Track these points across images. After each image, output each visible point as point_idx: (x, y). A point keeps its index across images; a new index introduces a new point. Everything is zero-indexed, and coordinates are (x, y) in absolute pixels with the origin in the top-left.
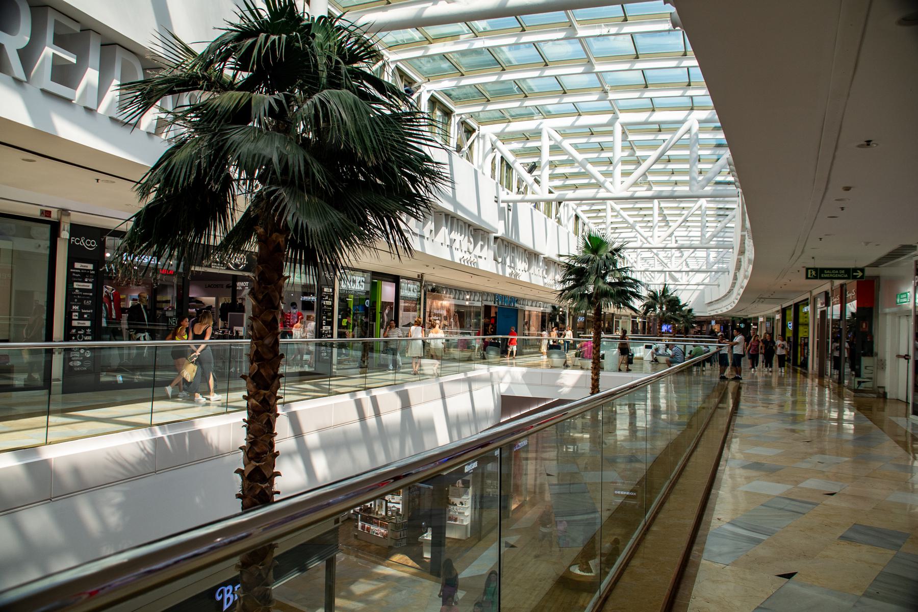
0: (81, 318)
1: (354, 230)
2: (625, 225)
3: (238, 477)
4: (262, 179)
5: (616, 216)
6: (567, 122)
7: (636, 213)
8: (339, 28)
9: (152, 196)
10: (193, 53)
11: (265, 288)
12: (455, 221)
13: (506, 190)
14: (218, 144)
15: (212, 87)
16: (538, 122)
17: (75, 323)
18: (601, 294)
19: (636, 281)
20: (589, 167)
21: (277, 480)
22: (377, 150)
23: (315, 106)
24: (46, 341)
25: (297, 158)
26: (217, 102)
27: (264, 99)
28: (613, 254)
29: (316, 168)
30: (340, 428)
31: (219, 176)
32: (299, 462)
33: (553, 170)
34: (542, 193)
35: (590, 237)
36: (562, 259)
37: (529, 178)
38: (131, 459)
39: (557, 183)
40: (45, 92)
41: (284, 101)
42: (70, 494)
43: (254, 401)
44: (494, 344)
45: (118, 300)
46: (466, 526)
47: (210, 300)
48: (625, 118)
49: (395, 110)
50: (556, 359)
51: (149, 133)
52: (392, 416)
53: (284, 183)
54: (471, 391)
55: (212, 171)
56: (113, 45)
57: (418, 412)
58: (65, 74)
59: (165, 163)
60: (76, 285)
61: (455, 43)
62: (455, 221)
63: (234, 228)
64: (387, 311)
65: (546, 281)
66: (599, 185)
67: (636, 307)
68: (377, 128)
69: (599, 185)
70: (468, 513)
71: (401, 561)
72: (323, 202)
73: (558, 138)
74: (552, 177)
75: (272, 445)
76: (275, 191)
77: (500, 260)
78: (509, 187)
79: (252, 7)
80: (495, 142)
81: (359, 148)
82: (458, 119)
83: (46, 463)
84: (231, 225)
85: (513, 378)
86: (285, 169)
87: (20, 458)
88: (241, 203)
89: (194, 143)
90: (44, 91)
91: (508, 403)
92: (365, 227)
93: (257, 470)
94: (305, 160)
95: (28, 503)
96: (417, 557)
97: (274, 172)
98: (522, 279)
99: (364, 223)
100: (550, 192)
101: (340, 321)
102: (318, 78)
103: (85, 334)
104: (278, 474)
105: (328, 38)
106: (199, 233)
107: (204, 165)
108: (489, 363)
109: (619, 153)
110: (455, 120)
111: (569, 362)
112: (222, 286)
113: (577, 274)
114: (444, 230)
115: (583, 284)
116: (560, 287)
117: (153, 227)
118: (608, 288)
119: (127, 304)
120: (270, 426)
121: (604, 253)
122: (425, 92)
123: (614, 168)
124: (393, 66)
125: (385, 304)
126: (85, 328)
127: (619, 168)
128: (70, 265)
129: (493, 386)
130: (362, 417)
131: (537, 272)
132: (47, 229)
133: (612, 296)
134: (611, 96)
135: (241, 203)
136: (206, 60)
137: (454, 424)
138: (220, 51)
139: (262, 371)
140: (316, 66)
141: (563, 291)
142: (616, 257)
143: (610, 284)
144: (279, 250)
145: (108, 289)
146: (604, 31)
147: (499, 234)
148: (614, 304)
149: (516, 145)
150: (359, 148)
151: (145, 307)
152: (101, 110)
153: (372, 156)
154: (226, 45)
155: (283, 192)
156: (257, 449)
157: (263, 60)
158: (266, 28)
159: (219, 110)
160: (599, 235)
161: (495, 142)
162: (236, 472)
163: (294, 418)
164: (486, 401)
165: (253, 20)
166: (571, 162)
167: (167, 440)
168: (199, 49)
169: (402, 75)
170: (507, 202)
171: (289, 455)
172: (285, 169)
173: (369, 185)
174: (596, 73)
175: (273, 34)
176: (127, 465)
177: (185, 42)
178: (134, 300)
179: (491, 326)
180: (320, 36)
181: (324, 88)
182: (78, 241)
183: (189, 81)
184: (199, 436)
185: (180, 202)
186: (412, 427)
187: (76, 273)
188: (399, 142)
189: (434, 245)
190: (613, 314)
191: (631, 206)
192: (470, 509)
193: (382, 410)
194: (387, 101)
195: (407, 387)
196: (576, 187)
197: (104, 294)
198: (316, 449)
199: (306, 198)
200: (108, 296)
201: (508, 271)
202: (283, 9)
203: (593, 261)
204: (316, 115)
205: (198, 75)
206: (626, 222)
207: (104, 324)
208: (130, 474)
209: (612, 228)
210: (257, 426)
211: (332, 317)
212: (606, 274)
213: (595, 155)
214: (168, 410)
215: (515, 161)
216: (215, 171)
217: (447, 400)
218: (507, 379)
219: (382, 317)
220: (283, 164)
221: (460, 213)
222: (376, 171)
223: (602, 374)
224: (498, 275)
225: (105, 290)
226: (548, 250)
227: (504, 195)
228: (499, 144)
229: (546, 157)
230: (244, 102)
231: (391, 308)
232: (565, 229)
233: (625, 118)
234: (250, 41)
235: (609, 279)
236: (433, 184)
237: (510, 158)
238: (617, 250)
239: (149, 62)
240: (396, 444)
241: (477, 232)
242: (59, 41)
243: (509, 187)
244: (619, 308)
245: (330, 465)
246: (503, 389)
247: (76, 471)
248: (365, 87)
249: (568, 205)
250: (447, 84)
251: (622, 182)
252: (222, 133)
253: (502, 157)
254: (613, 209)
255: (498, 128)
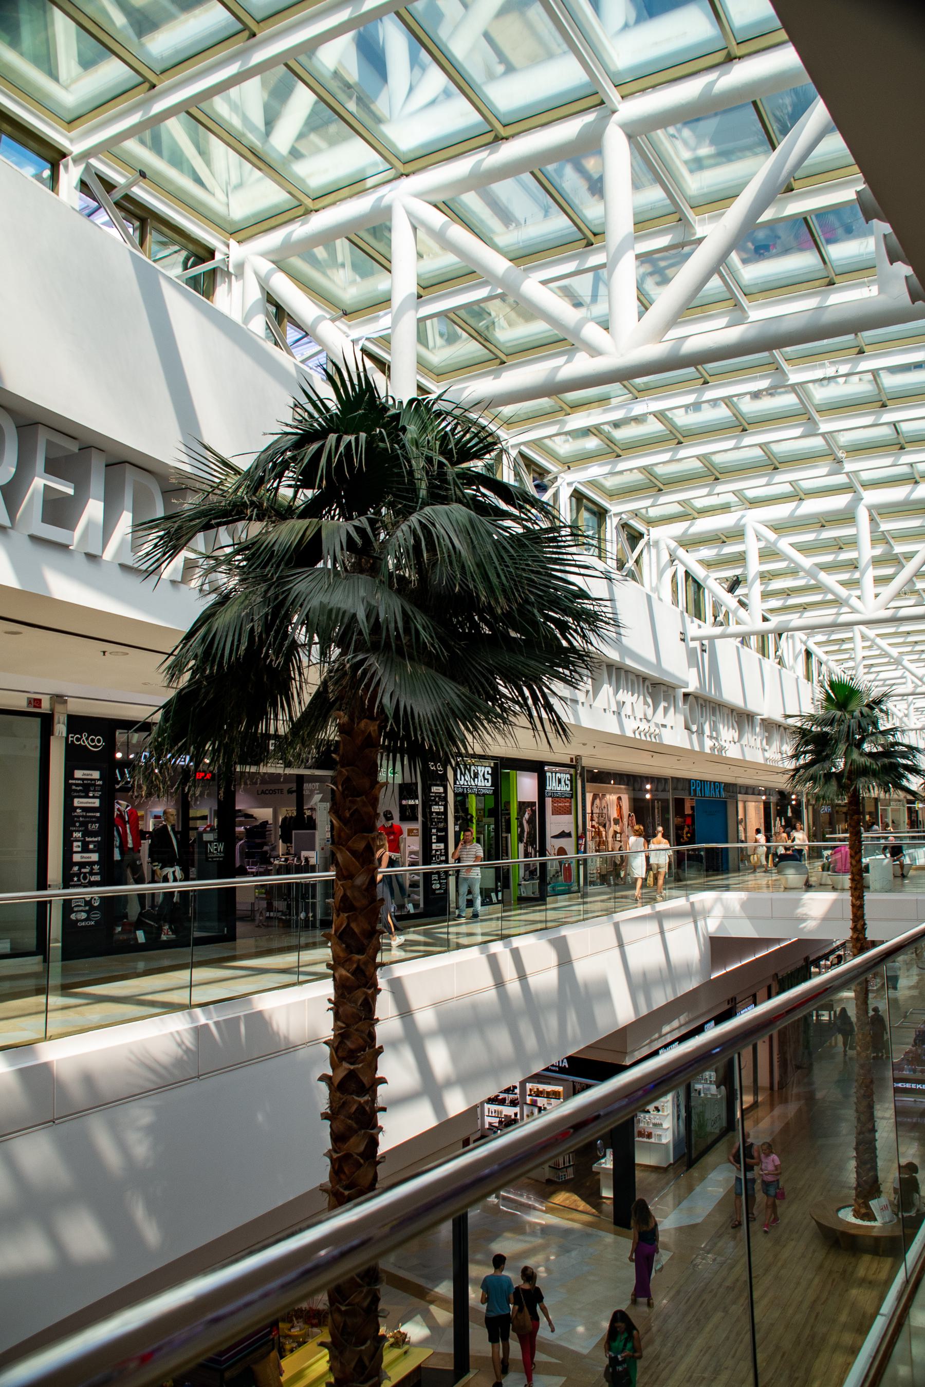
0: (85, 849)
1: (481, 706)
2: (886, 660)
3: (324, 1087)
4: (342, 642)
5: (870, 647)
6: (782, 511)
7: (901, 640)
8: (439, 414)
9: (187, 676)
10: (237, 472)
11: (353, 802)
12: (623, 673)
13: (696, 621)
14: (276, 598)
15: (264, 515)
16: (740, 514)
17: (77, 858)
18: (856, 772)
19: (910, 747)
20: (823, 576)
21: (381, 1089)
22: (509, 591)
23: (414, 532)
24: (39, 889)
25: (390, 607)
26: (272, 538)
27: (339, 527)
28: (872, 709)
29: (420, 621)
30: (467, 1000)
31: (281, 645)
32: (408, 1055)
33: (767, 584)
34: (752, 621)
35: (832, 685)
36: (791, 721)
37: (730, 601)
38: (164, 1059)
39: (775, 603)
40: (34, 538)
41: (369, 530)
42: (80, 1113)
43: (344, 972)
44: (695, 857)
45: (135, 819)
46: (666, 1145)
47: (264, 814)
48: (873, 497)
49: (529, 525)
50: (792, 876)
51: (173, 582)
52: (543, 973)
53: (375, 648)
54: (662, 932)
55: (271, 638)
56: (121, 467)
57: (584, 969)
58: (59, 511)
59: (202, 631)
60: (77, 802)
61: (605, 411)
62: (623, 673)
63: (303, 714)
64: (527, 816)
65: (767, 755)
66: (838, 602)
67: (914, 787)
68: (505, 556)
69: (838, 602)
70: (668, 1124)
71: (567, 1203)
72: (433, 672)
73: (771, 536)
74: (766, 595)
75: (372, 1036)
76: (363, 661)
77: (694, 728)
78: (698, 614)
79: (315, 398)
80: (675, 551)
81: (480, 587)
82: (615, 521)
83: (46, 1067)
84: (298, 711)
85: (726, 908)
86: (376, 627)
87: (11, 1061)
88: (311, 674)
89: (243, 598)
90: (33, 538)
91: (720, 948)
92: (494, 700)
93: (351, 1075)
94: (404, 612)
95: (24, 1128)
96: (592, 1196)
97: (360, 633)
98: (730, 754)
99: (494, 695)
100: (765, 619)
101: (457, 835)
102: (415, 490)
103: (92, 873)
104: (383, 1081)
105: (424, 429)
106: (254, 721)
107: (258, 630)
108: (686, 888)
109: (867, 551)
110: (611, 524)
111: (813, 880)
112: (281, 791)
113: (816, 742)
114: (607, 689)
115: (828, 757)
116: (791, 765)
117: (188, 717)
118: (868, 761)
119: (147, 824)
120: (368, 1007)
121: (857, 708)
122: (564, 486)
123: (863, 574)
124: (514, 453)
125: (523, 806)
126: (91, 864)
127: (871, 573)
128: (69, 775)
129: (695, 922)
130: (499, 983)
131: (752, 743)
132: (35, 724)
133: (875, 774)
134: (849, 467)
135: (311, 674)
136: (256, 479)
137: (639, 985)
138: (272, 465)
139: (353, 925)
140: (411, 473)
141: (797, 770)
142: (876, 711)
143: (871, 755)
144: (370, 743)
145: (122, 806)
146: (830, 371)
147: (690, 689)
148: (879, 785)
149: (707, 553)
150: (480, 587)
151: (173, 827)
152: (108, 555)
153: (502, 600)
154: (282, 453)
155: (374, 662)
156: (350, 1044)
157: (336, 475)
158: (337, 424)
159: (276, 548)
160: (846, 678)
161: (675, 551)
162: (321, 1079)
163: (397, 986)
164: (686, 946)
165: (316, 415)
166: (794, 572)
167: (213, 1028)
168: (244, 464)
169: (529, 463)
170: (700, 639)
171: (394, 1044)
172: (376, 627)
173: (499, 641)
174: (823, 435)
175: (347, 433)
176: (163, 1071)
177: (226, 454)
178: (156, 817)
179: (686, 829)
180: (412, 430)
181: (425, 504)
182: (78, 740)
183: (232, 510)
184: (259, 1020)
185: (226, 684)
186: (575, 993)
187: (77, 785)
188: (538, 573)
189: (597, 715)
190: (876, 800)
191: (892, 630)
192: (670, 1117)
193: (528, 970)
194: (516, 512)
195: (565, 931)
196: (804, 607)
197: (116, 812)
198: (433, 1034)
199: (409, 668)
200: (121, 816)
201: (708, 743)
202: (360, 396)
203: (841, 721)
204: (417, 547)
205: (246, 500)
206: (887, 655)
207: (117, 856)
208: (164, 1083)
209: (865, 666)
210: (349, 1008)
211: (445, 829)
212: (862, 741)
213: (810, 537)
214: (209, 982)
215: (707, 577)
216: (275, 638)
217: (627, 949)
218: (718, 911)
219: (521, 825)
220: (372, 620)
221: (629, 662)
222: (509, 619)
223: (868, 896)
224: (692, 751)
225: (117, 806)
226: (767, 707)
227: (694, 628)
228: (681, 552)
229: (754, 566)
230: (310, 534)
231: (533, 812)
232: (791, 673)
233: (873, 497)
234: (315, 446)
235: (867, 747)
236: (592, 630)
237: (700, 572)
238: (878, 702)
239: (172, 485)
240: (553, 1021)
241: (657, 689)
242: (52, 468)
243: (698, 614)
244: (887, 791)
245: (455, 1057)
246: (712, 926)
247: (88, 1080)
248: (484, 495)
249: (792, 637)
250: (595, 471)
251: (877, 596)
252: (282, 582)
253: (686, 572)
254: (864, 638)
255: (678, 528)
